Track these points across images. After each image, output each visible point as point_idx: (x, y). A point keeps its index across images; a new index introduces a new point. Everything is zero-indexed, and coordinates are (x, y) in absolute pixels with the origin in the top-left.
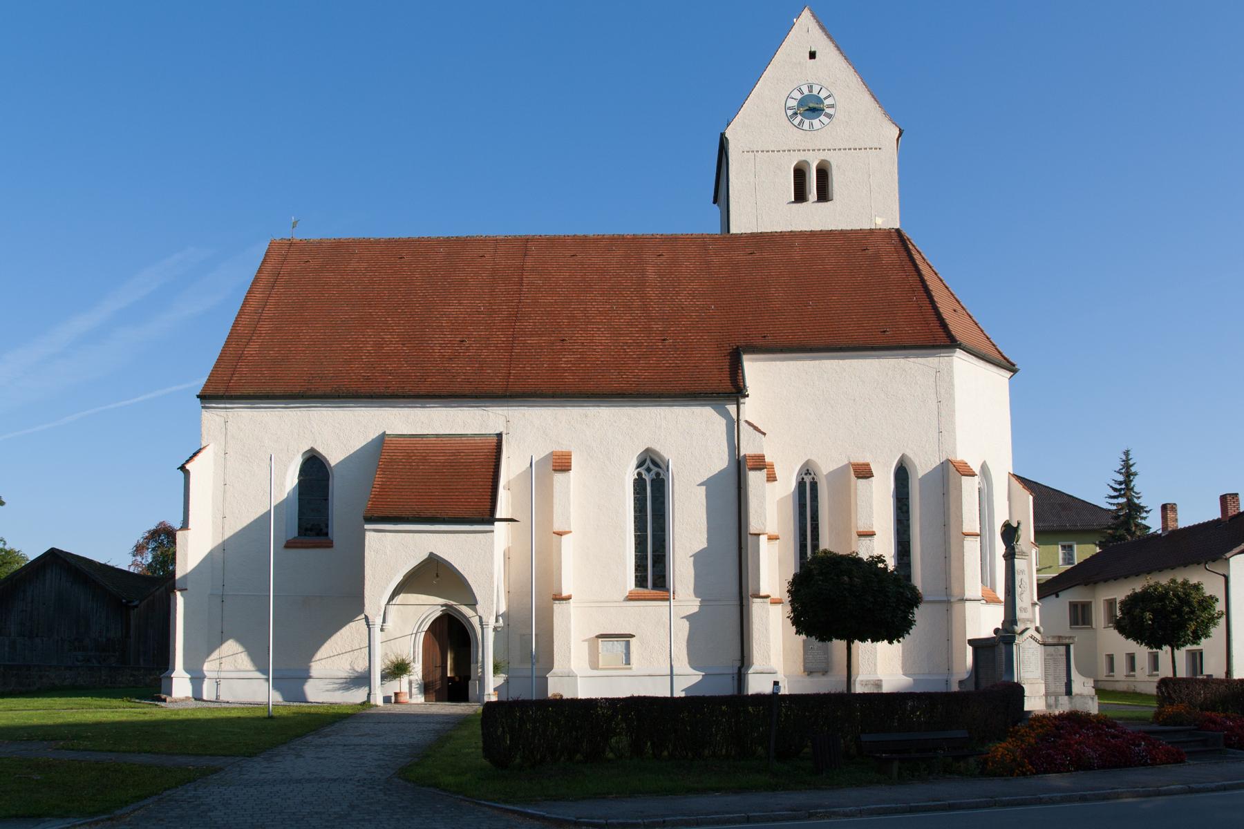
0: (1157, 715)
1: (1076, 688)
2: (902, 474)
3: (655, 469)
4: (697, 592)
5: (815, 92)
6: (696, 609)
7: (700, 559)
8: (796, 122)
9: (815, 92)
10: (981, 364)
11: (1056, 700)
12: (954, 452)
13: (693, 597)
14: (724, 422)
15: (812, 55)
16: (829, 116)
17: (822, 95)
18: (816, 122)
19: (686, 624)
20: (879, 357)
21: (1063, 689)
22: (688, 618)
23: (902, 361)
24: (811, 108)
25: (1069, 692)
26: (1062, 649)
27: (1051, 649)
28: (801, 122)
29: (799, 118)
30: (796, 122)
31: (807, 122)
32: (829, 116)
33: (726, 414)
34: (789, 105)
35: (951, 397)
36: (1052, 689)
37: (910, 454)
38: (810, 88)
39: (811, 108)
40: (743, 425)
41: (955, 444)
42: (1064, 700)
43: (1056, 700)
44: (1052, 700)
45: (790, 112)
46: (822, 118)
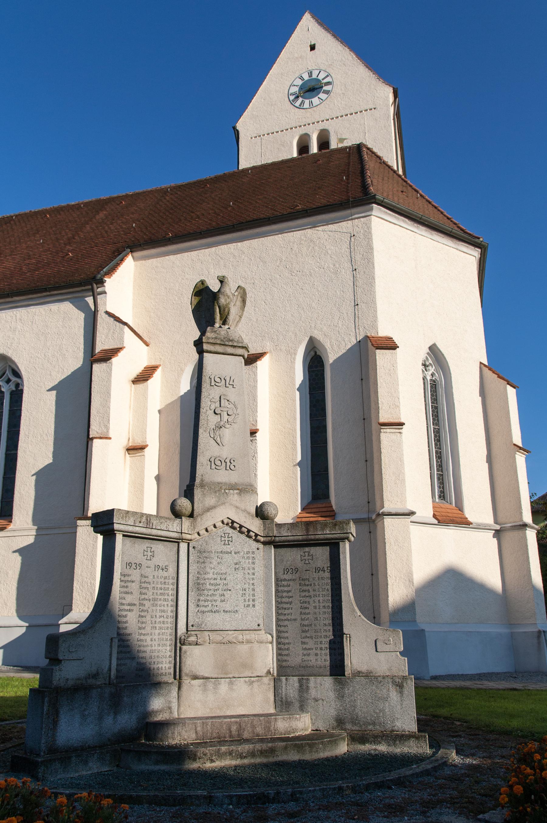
0: (500, 790)
1: (356, 656)
2: (315, 363)
3: (14, 379)
4: (35, 520)
5: (314, 76)
6: (31, 540)
7: (42, 477)
8: (298, 104)
9: (314, 76)
10: (422, 231)
11: (303, 688)
12: (374, 326)
13: (30, 525)
14: (82, 316)
15: (313, 48)
16: (327, 92)
17: (321, 77)
18: (315, 101)
19: (17, 559)
20: (281, 232)
21: (323, 659)
22: (20, 551)
23: (309, 232)
24: (311, 89)
25: (337, 668)
26: (321, 555)
27: (293, 556)
28: (303, 103)
29: (300, 99)
30: (298, 104)
31: (307, 102)
32: (327, 92)
33: (83, 307)
34: (291, 91)
35: (369, 261)
36: (296, 658)
37: (319, 336)
38: (310, 74)
39: (311, 89)
40: (102, 318)
41: (375, 317)
42: (323, 686)
43: (303, 688)
44: (291, 687)
45: (292, 98)
46: (322, 96)
